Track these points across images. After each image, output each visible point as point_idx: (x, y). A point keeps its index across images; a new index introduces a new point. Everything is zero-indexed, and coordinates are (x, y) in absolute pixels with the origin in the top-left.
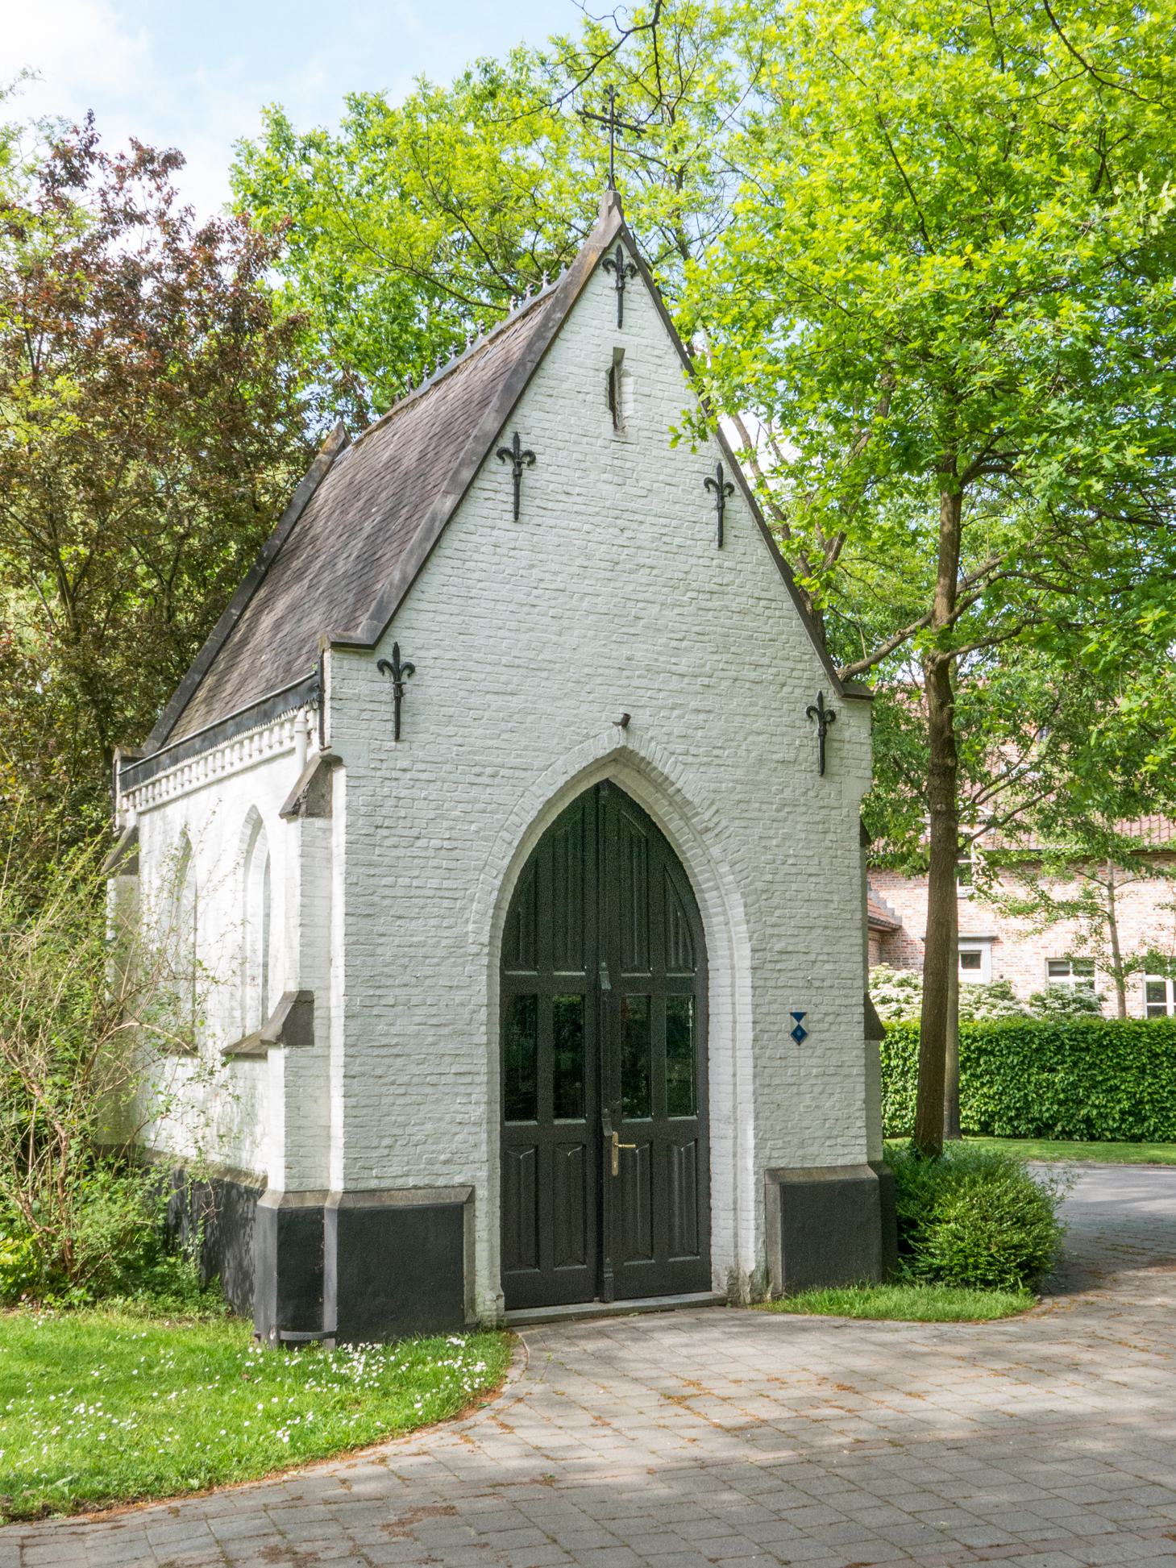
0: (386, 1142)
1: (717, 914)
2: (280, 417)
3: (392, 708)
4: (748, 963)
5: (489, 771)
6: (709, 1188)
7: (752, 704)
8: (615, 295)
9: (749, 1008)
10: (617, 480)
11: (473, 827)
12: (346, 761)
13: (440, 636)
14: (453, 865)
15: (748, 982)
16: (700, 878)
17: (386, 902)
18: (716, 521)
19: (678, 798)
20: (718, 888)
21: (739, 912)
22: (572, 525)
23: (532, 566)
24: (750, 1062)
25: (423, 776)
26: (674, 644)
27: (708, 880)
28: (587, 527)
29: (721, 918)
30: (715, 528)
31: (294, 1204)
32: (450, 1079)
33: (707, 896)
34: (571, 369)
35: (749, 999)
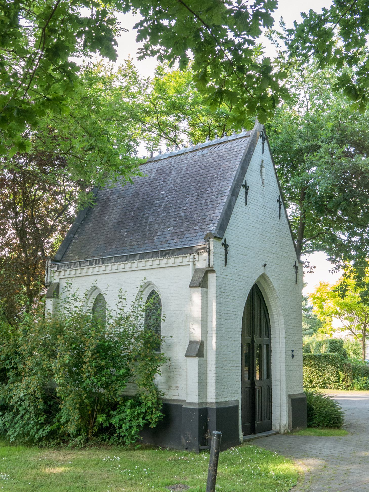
0: (223, 387)
1: (276, 322)
2: (28, 278)
3: (224, 257)
4: (284, 336)
5: (241, 277)
6: (271, 400)
7: (285, 263)
8: (262, 144)
9: (284, 349)
10: (262, 197)
11: (239, 293)
12: (216, 272)
13: (232, 237)
14: (236, 305)
15: (284, 341)
16: (273, 311)
17: (223, 315)
18: (279, 211)
19: (272, 288)
20: (277, 314)
21: (283, 321)
22: (256, 208)
23: (248, 219)
24: (285, 364)
25: (230, 278)
26: (272, 244)
27: (275, 312)
28: (258, 209)
29: (277, 323)
30: (278, 213)
31: (201, 407)
32: (234, 368)
33: (274, 316)
34: (255, 164)
35: (284, 346)
